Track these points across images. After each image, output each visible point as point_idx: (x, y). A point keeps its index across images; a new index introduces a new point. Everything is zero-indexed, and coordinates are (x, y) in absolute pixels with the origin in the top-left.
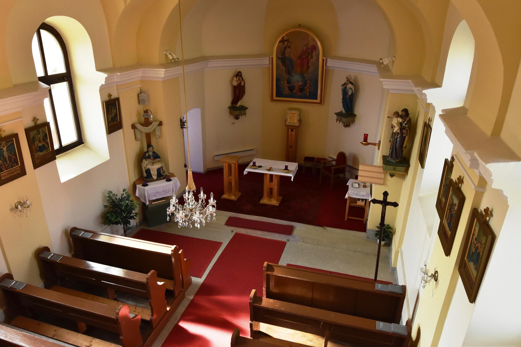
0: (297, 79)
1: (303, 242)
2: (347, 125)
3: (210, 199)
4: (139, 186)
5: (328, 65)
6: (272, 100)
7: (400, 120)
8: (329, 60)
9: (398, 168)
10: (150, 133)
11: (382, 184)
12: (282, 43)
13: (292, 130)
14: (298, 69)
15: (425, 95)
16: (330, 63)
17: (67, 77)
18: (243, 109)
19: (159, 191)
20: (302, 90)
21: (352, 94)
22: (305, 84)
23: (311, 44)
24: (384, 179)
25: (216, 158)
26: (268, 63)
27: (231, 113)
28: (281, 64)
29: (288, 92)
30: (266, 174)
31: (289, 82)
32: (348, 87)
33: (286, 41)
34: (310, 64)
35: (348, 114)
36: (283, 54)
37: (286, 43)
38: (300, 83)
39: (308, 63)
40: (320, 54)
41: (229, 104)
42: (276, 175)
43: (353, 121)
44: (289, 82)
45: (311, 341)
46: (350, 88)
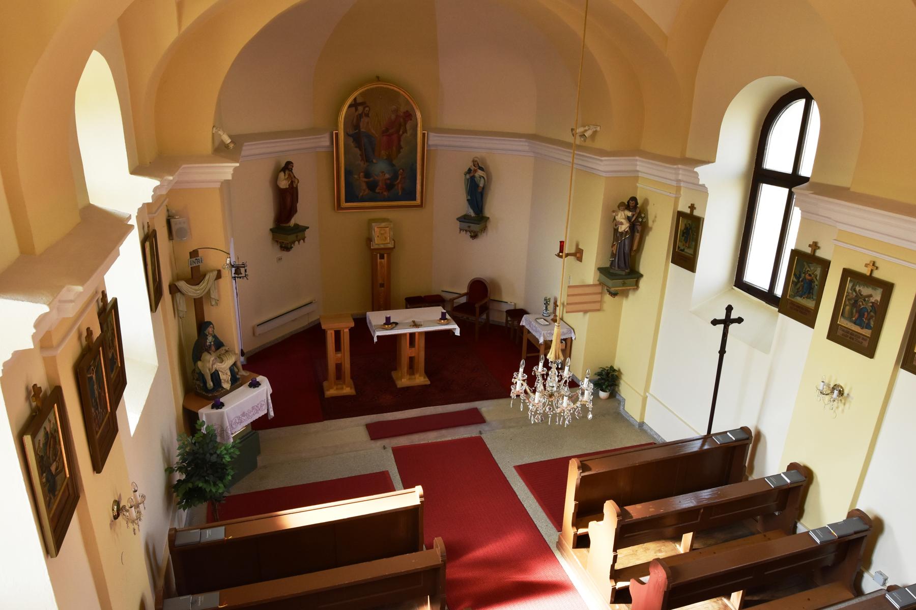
0: (381, 169)
1: (504, 428)
2: (474, 236)
3: (518, 371)
4: (206, 413)
5: (430, 143)
6: (421, 206)
7: (630, 214)
8: (432, 134)
9: (627, 281)
10: (201, 298)
11: (599, 310)
12: (353, 109)
13: (382, 257)
14: (383, 152)
15: (696, 173)
16: (434, 139)
17: (759, 175)
18: (300, 230)
19: (246, 411)
20: (390, 186)
21: (483, 188)
22: (395, 176)
23: (403, 109)
24: (601, 302)
25: (259, 330)
26: (328, 143)
27: (275, 239)
28: (352, 145)
29: (367, 191)
30: (405, 334)
31: (367, 175)
32: (477, 175)
33: (361, 104)
34: (402, 144)
35: (476, 220)
36: (357, 126)
37: (360, 109)
38: (387, 176)
39: (399, 140)
40: (419, 125)
41: (271, 225)
42: (420, 333)
43: (484, 229)
44: (367, 175)
45: (660, 551)
46: (480, 177)
